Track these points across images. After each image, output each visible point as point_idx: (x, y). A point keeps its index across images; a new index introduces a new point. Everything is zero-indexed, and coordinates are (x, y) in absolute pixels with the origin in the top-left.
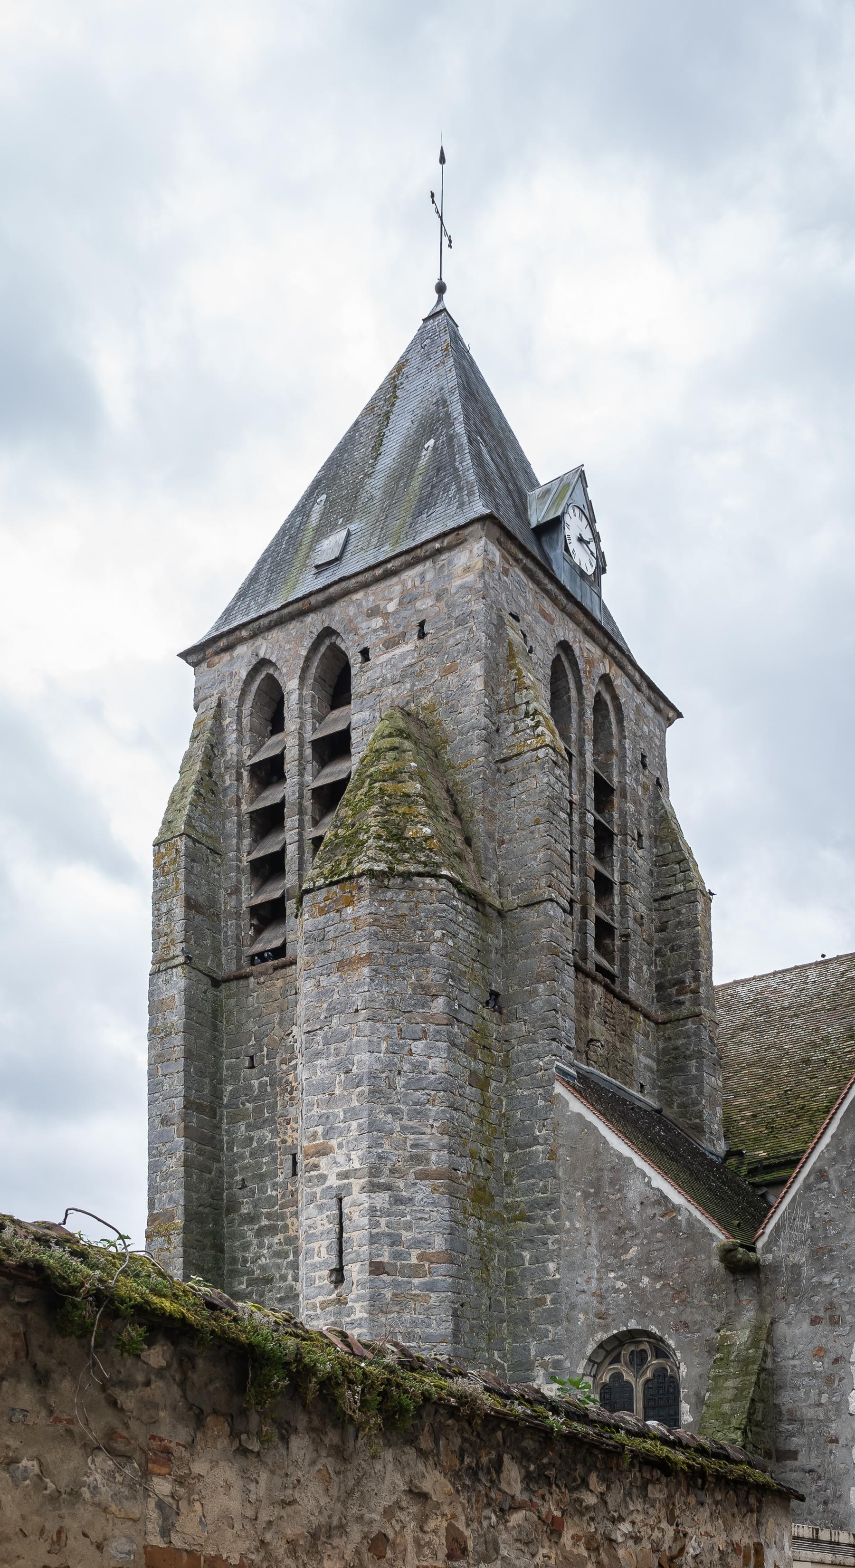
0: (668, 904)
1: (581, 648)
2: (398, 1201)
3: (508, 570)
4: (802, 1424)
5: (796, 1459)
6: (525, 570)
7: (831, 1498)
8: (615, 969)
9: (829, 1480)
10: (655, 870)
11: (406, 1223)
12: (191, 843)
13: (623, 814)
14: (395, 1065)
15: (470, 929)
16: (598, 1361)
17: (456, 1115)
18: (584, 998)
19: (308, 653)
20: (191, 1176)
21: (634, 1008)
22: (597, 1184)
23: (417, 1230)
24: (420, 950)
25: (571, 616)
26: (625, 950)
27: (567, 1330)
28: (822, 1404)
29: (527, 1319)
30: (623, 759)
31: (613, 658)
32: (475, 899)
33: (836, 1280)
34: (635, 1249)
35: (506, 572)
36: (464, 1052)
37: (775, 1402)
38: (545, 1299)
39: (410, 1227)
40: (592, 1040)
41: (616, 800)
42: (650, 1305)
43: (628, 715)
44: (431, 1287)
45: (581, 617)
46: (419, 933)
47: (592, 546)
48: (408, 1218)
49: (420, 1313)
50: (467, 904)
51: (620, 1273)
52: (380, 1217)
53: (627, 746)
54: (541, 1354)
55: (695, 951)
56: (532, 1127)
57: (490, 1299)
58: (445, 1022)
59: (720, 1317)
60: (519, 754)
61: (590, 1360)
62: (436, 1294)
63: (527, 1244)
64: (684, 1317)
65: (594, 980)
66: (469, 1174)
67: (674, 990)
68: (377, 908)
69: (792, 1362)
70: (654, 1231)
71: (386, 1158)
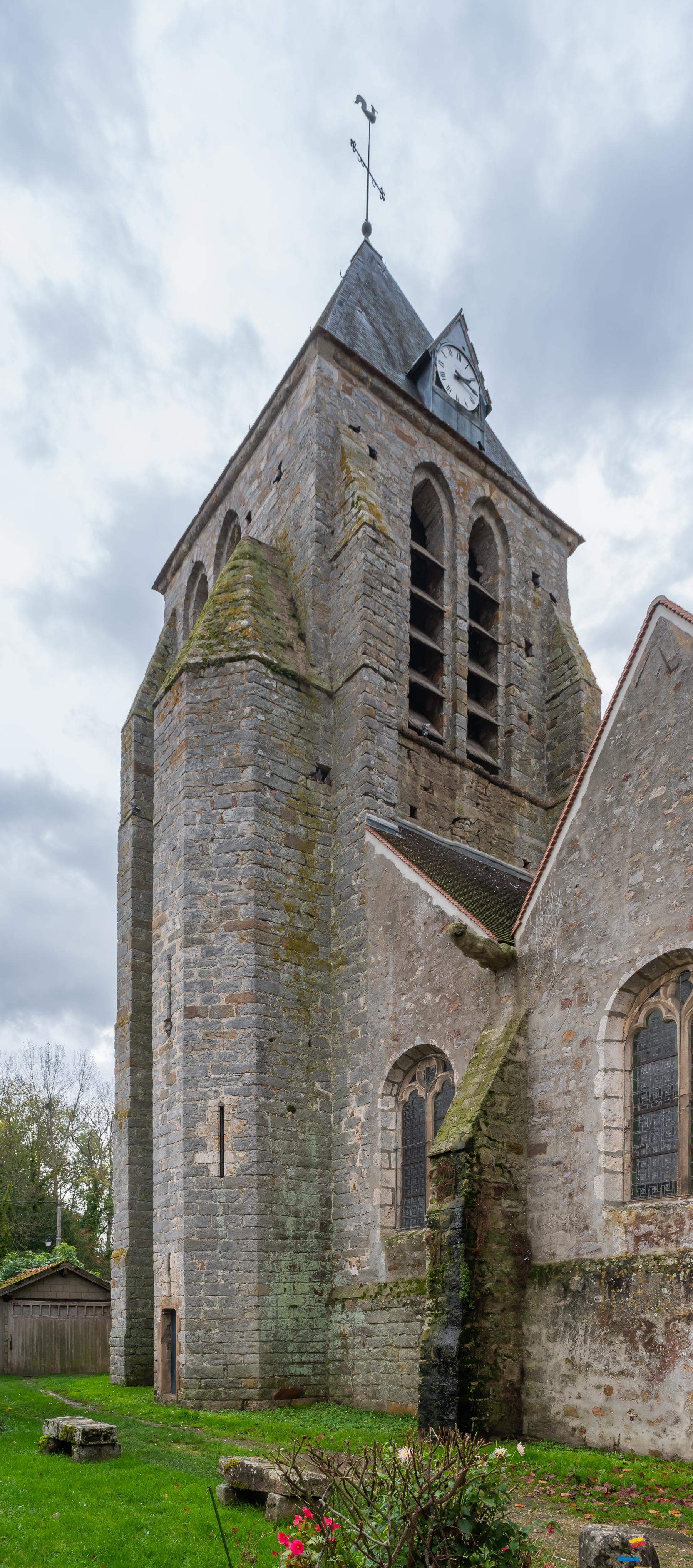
0: (557, 701)
1: (452, 471)
2: (210, 952)
3: (351, 389)
4: (551, 1115)
5: (545, 1153)
6: (375, 390)
7: (576, 1190)
8: (499, 763)
9: (575, 1171)
10: (548, 676)
11: (215, 971)
12: (140, 722)
13: (508, 624)
14: (208, 833)
15: (288, 707)
16: (398, 1081)
17: (266, 872)
18: (449, 781)
19: (219, 540)
20: (140, 978)
21: (518, 794)
22: (393, 917)
23: (226, 976)
24: (231, 729)
25: (438, 439)
26: (508, 745)
27: (372, 1056)
28: (569, 1091)
29: (345, 1051)
30: (508, 576)
31: (495, 482)
32: (300, 682)
33: (585, 956)
34: (420, 969)
35: (348, 391)
36: (280, 817)
37: (529, 1096)
38: (357, 1031)
39: (220, 974)
40: (458, 819)
41: (500, 614)
42: (431, 1019)
43: (514, 536)
44: (237, 1026)
45: (449, 439)
46: (230, 712)
47: (475, 385)
48: (218, 966)
49: (227, 1049)
50: (284, 684)
51: (410, 994)
52: (193, 968)
53: (512, 563)
54: (354, 1081)
55: (578, 735)
56: (350, 878)
57: (310, 1036)
58: (253, 788)
59: (484, 1018)
60: (346, 544)
61: (388, 1080)
62: (242, 1031)
63: (346, 985)
64: (456, 1026)
65: (463, 765)
66: (283, 925)
67: (561, 776)
68: (193, 697)
69: (544, 1052)
70: (434, 948)
71: (199, 916)
